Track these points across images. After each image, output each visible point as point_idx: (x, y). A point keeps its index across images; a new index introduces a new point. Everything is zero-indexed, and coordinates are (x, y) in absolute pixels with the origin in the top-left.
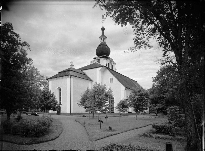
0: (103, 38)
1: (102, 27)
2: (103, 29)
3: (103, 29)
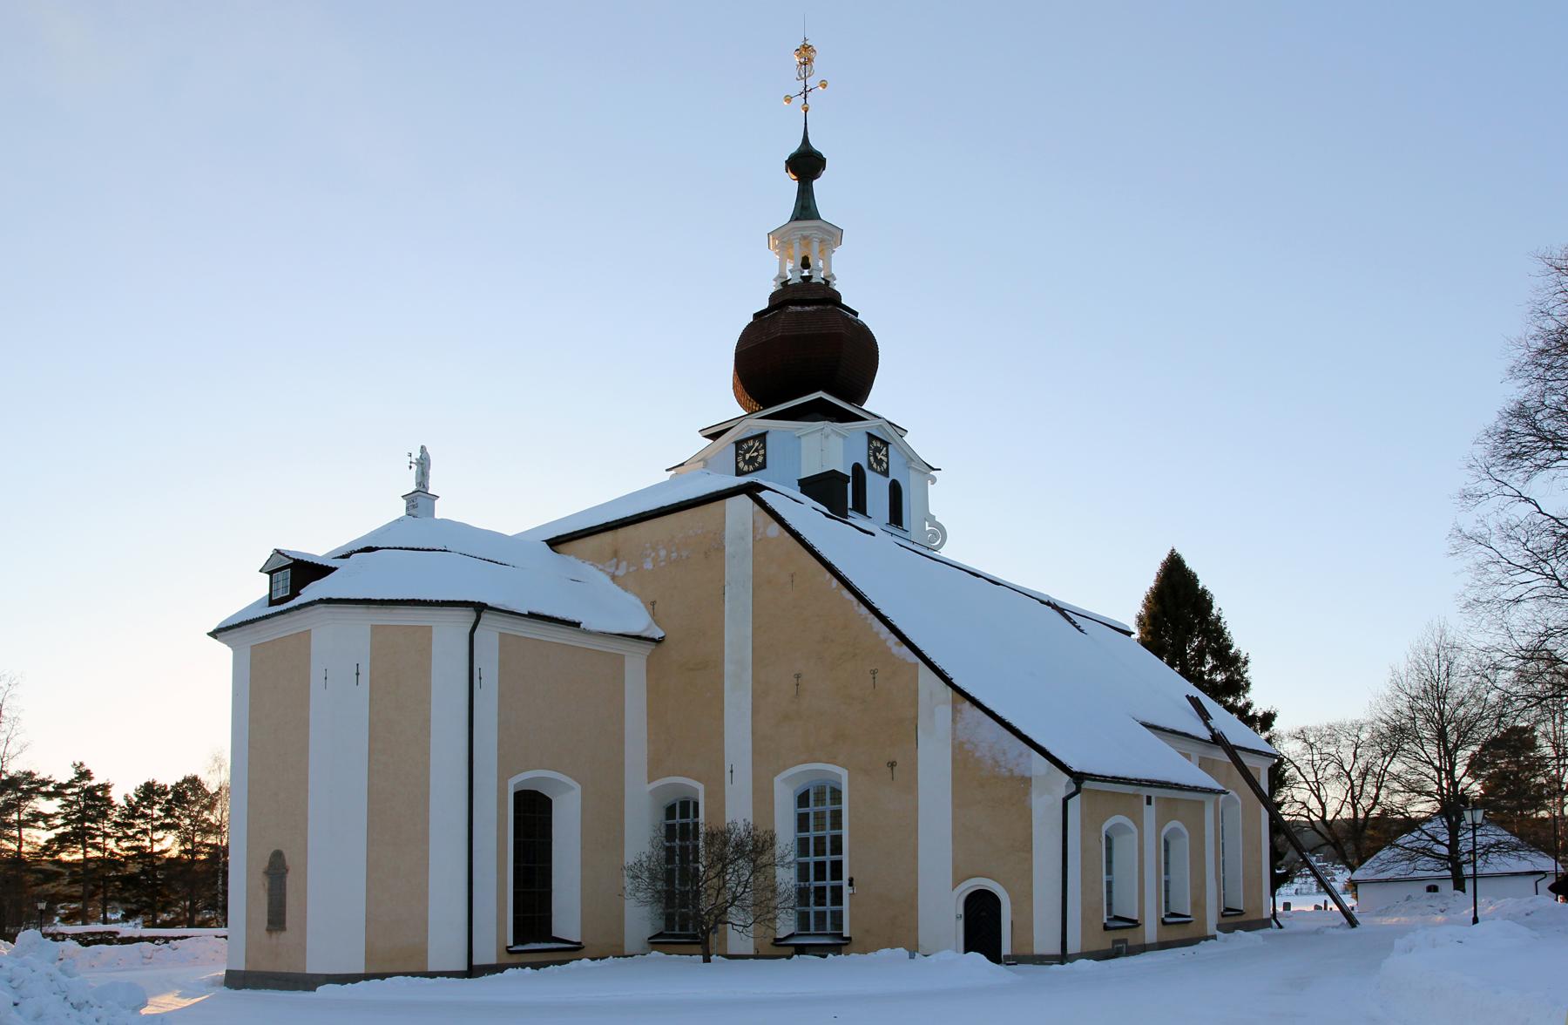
1: (794, 146)
2: (806, 164)
3: (806, 164)
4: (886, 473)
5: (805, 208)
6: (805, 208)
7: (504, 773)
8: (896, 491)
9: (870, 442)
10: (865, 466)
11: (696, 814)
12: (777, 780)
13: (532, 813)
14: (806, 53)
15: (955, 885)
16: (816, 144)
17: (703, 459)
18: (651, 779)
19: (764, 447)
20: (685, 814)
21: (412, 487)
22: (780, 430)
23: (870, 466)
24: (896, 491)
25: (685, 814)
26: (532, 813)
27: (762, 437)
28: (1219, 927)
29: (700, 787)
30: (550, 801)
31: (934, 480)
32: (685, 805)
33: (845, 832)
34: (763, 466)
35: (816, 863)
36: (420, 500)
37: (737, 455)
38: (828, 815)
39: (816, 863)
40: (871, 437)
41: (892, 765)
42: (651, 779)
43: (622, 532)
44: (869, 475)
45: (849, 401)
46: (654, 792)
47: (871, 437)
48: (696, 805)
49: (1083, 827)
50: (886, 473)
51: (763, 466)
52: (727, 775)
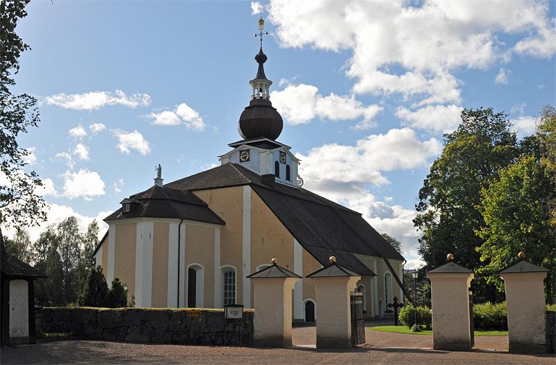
0: (261, 85)
1: (258, 52)
2: (261, 58)
3: (261, 58)
4: (285, 163)
5: (261, 73)
6: (261, 73)
7: (187, 263)
8: (288, 167)
13: (192, 273)
16: (265, 53)
17: (230, 155)
18: (221, 265)
20: (230, 276)
21: (156, 177)
22: (254, 150)
24: (288, 167)
25: (230, 276)
26: (192, 273)
27: (248, 151)
28: (405, 319)
29: (236, 268)
32: (230, 273)
34: (248, 160)
36: (159, 179)
40: (281, 152)
42: (221, 265)
43: (213, 191)
44: (280, 164)
45: (211, 308)
46: (222, 269)
48: (234, 273)
49: (167, 249)
50: (285, 163)
52: (152, 236)
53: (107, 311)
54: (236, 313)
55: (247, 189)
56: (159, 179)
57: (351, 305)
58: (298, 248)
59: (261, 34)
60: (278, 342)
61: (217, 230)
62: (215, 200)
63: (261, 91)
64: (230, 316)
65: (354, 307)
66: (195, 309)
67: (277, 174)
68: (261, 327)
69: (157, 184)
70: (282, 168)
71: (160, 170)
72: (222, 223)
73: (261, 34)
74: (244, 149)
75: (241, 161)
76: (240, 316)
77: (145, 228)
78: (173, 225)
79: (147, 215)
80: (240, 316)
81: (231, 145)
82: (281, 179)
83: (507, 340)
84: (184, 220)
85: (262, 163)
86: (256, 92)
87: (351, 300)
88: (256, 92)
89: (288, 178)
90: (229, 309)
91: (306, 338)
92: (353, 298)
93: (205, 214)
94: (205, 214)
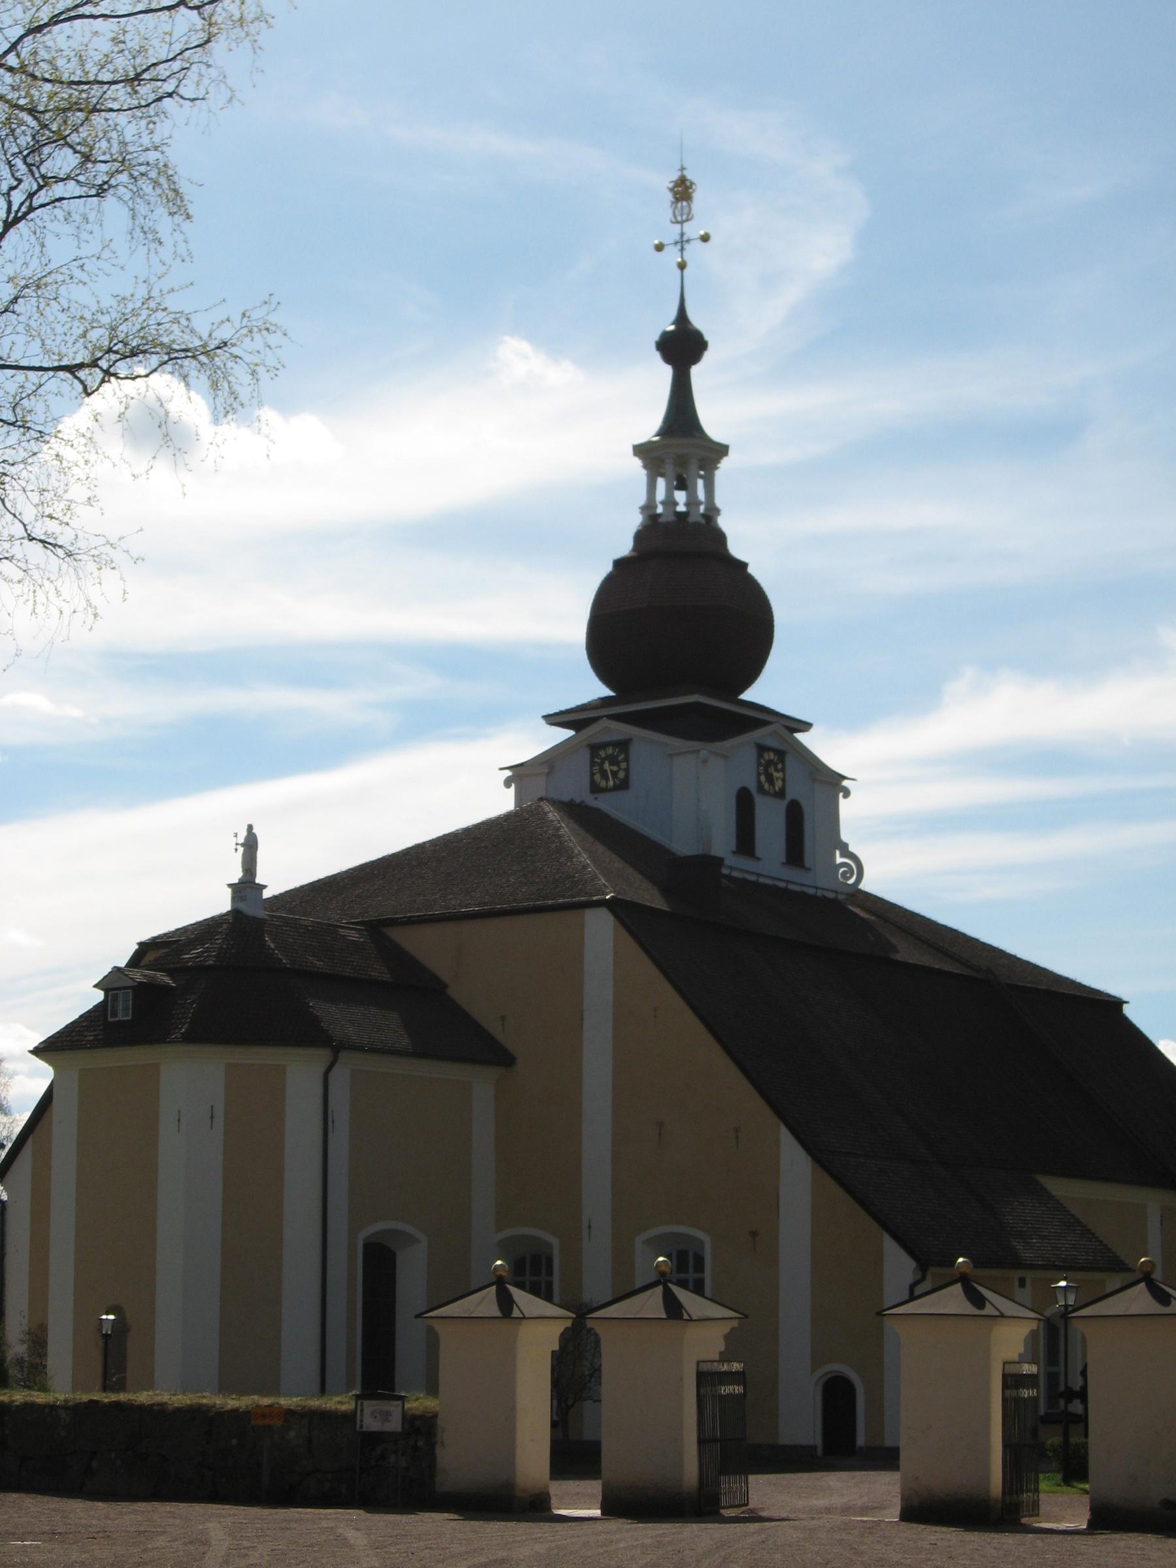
1: (675, 176)
3: (682, 347)
4: (781, 794)
5: (681, 412)
6: (681, 412)
9: (760, 756)
10: (753, 788)
11: (550, 1272)
12: (639, 1240)
13: (379, 1262)
14: (682, 191)
15: (813, 1370)
16: (697, 320)
17: (548, 762)
19: (627, 760)
23: (761, 789)
26: (379, 1262)
27: (624, 745)
30: (394, 1254)
31: (847, 793)
33: (708, 1276)
34: (623, 785)
35: (687, 1272)
37: (593, 764)
38: (691, 1270)
39: (687, 1272)
40: (762, 749)
41: (754, 1234)
44: (759, 800)
47: (762, 749)
50: (781, 794)
51: (623, 785)
53: (987, 1451)
54: (386, 1416)
55: (600, 928)
56: (246, 888)
57: (1004, 1400)
58: (794, 1166)
59: (682, 242)
60: (536, 1508)
61: (481, 1084)
62: (475, 966)
63: (682, 485)
64: (370, 1424)
65: (1010, 1407)
66: (284, 1402)
67: (746, 842)
68: (456, 1460)
69: (242, 906)
70: (770, 821)
71: (250, 845)
72: (495, 1055)
73: (682, 242)
74: (606, 738)
75: (595, 789)
76: (395, 1425)
77: (190, 1081)
78: (300, 1073)
79: (192, 1038)
80: (395, 1425)
81: (556, 719)
82: (770, 860)
83: (896, 1490)
84: (343, 1055)
85: (688, 795)
86: (661, 494)
87: (1005, 1386)
88: (661, 494)
89: (795, 854)
90: (369, 1406)
91: (579, 1504)
92: (705, 1378)
93: (446, 1030)
94: (446, 1030)
